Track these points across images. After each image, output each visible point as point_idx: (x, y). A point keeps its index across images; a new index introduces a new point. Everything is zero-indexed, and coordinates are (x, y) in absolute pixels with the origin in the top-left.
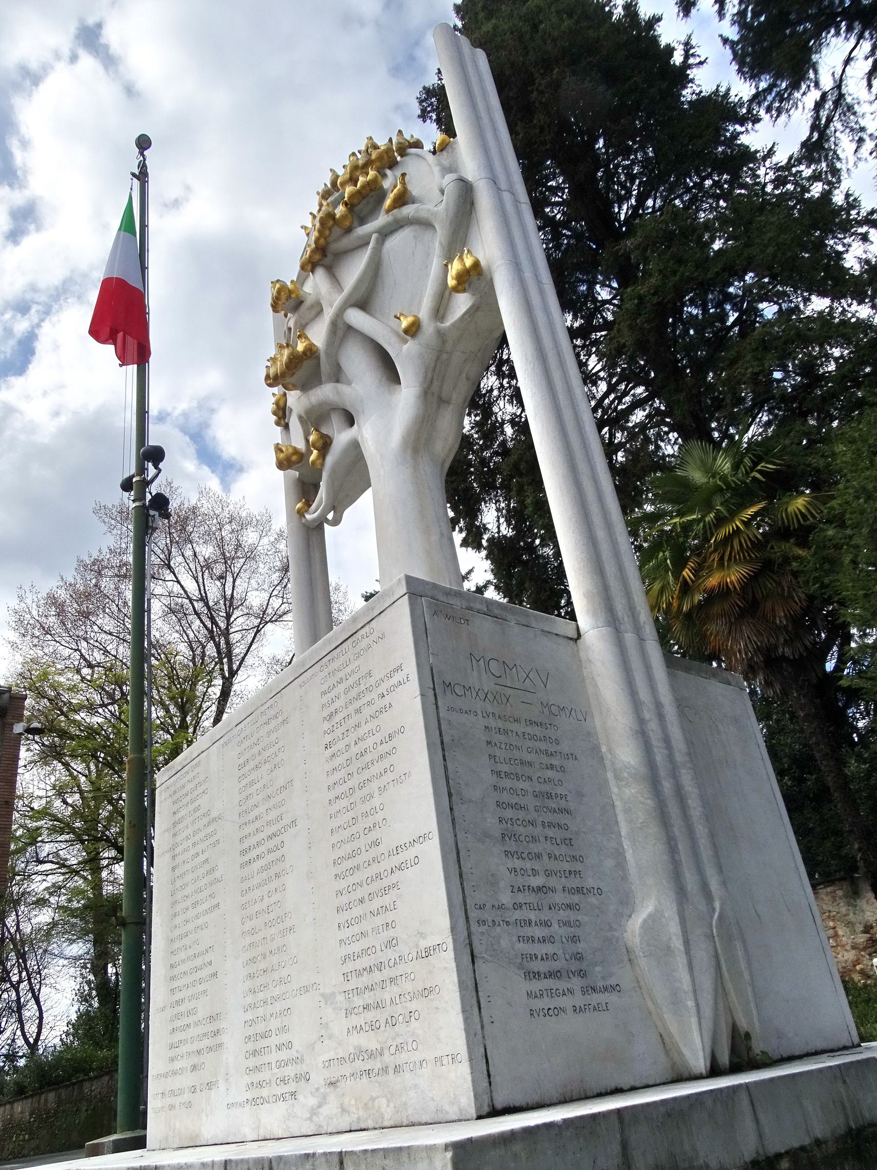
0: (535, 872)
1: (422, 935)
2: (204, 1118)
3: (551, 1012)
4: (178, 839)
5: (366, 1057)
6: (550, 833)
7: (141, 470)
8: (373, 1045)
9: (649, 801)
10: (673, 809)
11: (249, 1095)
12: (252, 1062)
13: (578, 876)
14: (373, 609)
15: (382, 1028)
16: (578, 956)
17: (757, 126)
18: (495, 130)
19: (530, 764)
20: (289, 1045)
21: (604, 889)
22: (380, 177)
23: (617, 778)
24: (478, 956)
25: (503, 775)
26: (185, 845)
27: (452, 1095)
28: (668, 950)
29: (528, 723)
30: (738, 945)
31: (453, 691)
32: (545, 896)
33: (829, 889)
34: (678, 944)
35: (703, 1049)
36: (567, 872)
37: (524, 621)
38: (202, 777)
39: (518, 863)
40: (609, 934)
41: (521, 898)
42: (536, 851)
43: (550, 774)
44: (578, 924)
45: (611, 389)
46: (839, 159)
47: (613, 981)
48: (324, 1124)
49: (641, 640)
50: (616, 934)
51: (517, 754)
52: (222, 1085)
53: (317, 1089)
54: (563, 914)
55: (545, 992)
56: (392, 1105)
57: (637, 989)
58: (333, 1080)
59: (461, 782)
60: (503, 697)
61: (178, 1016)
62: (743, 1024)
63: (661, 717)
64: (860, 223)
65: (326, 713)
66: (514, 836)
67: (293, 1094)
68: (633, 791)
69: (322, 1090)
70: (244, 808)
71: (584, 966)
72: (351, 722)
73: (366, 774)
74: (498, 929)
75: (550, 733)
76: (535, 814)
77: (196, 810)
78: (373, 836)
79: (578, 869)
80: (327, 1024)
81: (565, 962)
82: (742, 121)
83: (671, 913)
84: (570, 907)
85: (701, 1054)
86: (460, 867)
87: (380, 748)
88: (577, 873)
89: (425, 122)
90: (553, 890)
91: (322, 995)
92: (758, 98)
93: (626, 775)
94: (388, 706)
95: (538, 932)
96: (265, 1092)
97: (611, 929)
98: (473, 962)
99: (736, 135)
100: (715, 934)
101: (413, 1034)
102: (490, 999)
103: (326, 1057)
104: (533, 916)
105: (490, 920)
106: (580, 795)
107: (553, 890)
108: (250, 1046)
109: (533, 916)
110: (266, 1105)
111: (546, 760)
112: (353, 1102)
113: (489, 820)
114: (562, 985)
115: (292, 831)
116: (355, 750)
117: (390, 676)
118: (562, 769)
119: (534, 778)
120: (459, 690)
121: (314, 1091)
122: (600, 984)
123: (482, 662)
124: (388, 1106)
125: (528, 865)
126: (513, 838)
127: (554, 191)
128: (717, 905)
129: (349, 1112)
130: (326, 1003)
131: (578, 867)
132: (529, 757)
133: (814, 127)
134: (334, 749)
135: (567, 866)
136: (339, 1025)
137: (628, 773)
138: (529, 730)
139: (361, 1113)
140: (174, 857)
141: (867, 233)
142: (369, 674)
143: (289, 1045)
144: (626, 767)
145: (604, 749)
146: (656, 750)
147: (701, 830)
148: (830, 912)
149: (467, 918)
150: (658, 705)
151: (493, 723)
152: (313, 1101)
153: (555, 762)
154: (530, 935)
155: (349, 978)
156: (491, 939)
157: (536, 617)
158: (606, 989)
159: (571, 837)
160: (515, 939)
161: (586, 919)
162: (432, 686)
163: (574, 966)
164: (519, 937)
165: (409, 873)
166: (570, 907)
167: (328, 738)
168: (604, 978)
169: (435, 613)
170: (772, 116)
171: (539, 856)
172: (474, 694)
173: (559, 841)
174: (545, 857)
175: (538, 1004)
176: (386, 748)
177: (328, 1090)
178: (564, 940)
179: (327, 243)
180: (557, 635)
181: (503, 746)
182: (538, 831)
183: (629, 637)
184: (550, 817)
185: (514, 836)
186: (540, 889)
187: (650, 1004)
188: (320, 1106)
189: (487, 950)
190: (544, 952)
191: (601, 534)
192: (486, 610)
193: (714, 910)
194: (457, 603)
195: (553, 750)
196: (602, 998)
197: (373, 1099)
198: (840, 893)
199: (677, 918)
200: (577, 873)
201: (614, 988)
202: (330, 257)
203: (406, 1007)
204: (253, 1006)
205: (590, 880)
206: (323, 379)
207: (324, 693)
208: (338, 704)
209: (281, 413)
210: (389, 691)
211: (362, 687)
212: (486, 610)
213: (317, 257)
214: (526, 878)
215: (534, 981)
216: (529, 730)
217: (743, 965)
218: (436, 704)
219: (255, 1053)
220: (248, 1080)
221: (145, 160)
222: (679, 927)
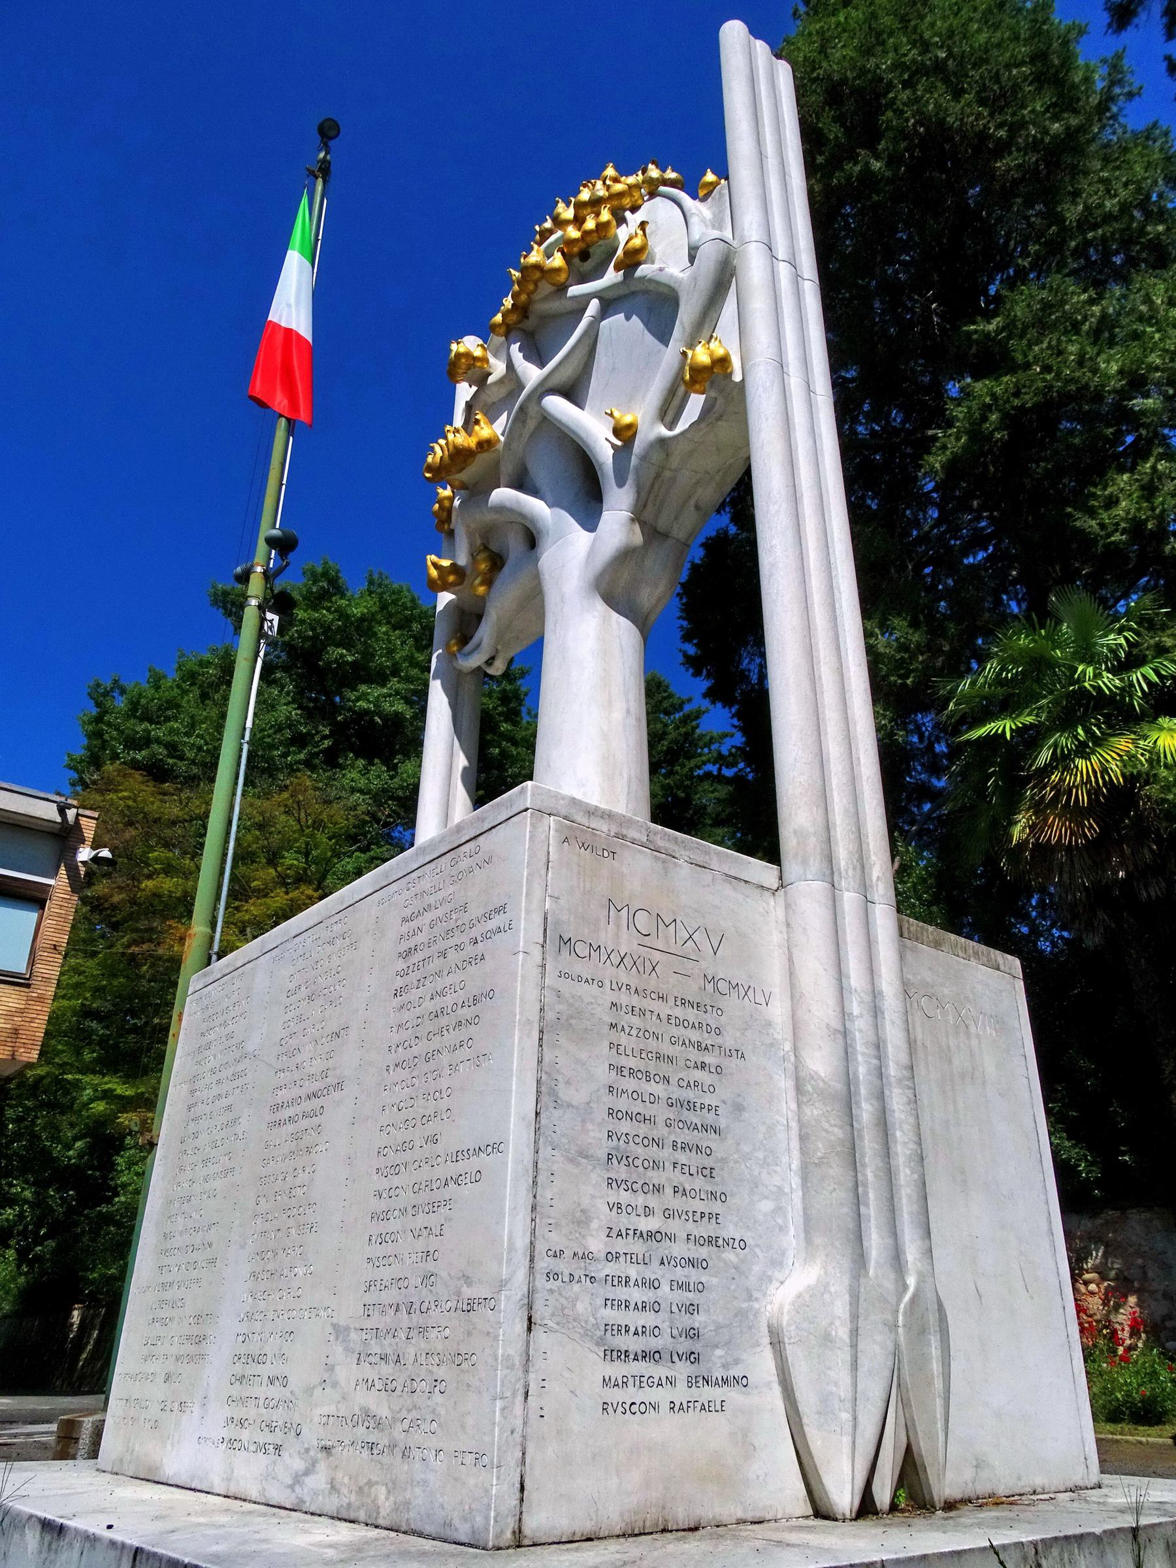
0: (648, 1211)
1: (468, 1280)
2: (169, 1447)
5: (372, 1425)
6: (682, 1157)
8: (384, 1412)
9: (836, 1130)
10: (869, 1144)
11: (225, 1433)
12: (236, 1390)
14: (483, 820)
15: (398, 1392)
16: (692, 1332)
20: (284, 1381)
21: (750, 1242)
22: (614, 223)
24: (539, 1322)
25: (626, 1073)
27: (467, 1507)
29: (679, 1003)
30: (934, 1341)
34: (842, 1332)
36: (698, 1215)
37: (700, 859)
39: (624, 1197)
40: (745, 1305)
41: (620, 1246)
43: (698, 1075)
47: (737, 1372)
48: (307, 1499)
49: (867, 901)
50: (756, 1306)
51: (652, 1044)
52: (196, 1409)
53: (307, 1450)
54: (680, 1274)
55: (631, 1380)
56: (392, 1499)
58: (329, 1443)
59: (560, 1078)
60: (647, 963)
61: (163, 1303)
63: (876, 1011)
66: (628, 1160)
67: (278, 1448)
68: (815, 1112)
69: (312, 1453)
71: (698, 1347)
72: (432, 967)
73: (436, 1042)
74: (576, 1287)
75: (710, 1019)
77: (230, 1036)
78: (431, 1128)
79: (715, 1210)
80: (333, 1366)
81: (671, 1340)
83: (840, 1286)
84: (691, 1262)
85: (849, 1487)
87: (460, 1011)
88: (714, 1217)
90: (671, 1238)
91: (334, 1326)
94: (479, 957)
95: (637, 1295)
96: (245, 1435)
97: (750, 1298)
98: (529, 1329)
100: (900, 1323)
101: (434, 1411)
102: (544, 1384)
103: (326, 1410)
104: (633, 1272)
105: (566, 1273)
106: (739, 1108)
107: (671, 1238)
108: (238, 1369)
109: (633, 1272)
110: (243, 1453)
111: (694, 1055)
112: (346, 1480)
113: (592, 1134)
115: (336, 1095)
116: (429, 1006)
118: (719, 1071)
119: (673, 1081)
120: (582, 949)
121: (302, 1451)
122: (718, 1373)
123: (624, 912)
124: (387, 1499)
125: (640, 1200)
126: (624, 1161)
128: (911, 1281)
129: (339, 1493)
130: (337, 1338)
131: (717, 1207)
132: (670, 1050)
134: (405, 998)
135: (699, 1206)
136: (347, 1372)
137: (812, 1086)
138: (678, 1012)
139: (353, 1498)
140: (193, 1092)
143: (284, 1381)
144: (812, 1077)
146: (860, 1058)
147: (905, 1175)
148: (1140, 1245)
149: (531, 1268)
150: (875, 995)
151: (624, 999)
152: (298, 1465)
153: (709, 1059)
154: (623, 1298)
155: (371, 1312)
156: (563, 1301)
157: (718, 854)
158: (725, 1381)
160: (600, 1302)
161: (715, 1281)
162: (541, 941)
163: (684, 1346)
165: (467, 1190)
166: (691, 1262)
167: (399, 982)
168: (725, 1366)
169: (566, 840)
171: (658, 1189)
172: (604, 957)
174: (669, 1191)
175: (617, 1395)
176: (465, 1013)
177: (320, 1455)
178: (675, 1309)
179: (530, 301)
182: (666, 1154)
183: (850, 899)
184: (686, 1136)
185: (628, 1160)
186: (651, 1235)
188: (307, 1473)
189: (553, 1315)
190: (641, 1323)
191: (834, 749)
192: (644, 839)
193: (905, 1287)
194: (603, 826)
195: (709, 1042)
197: (370, 1484)
199: (847, 1297)
200: (714, 1217)
203: (431, 1372)
205: (731, 1227)
206: (502, 481)
207: (405, 920)
208: (421, 938)
210: (486, 937)
211: (452, 924)
212: (644, 839)
215: (617, 1363)
216: (678, 1012)
217: (936, 1366)
218: (543, 966)
219: (241, 1379)
220: (228, 1412)
222: (848, 1308)
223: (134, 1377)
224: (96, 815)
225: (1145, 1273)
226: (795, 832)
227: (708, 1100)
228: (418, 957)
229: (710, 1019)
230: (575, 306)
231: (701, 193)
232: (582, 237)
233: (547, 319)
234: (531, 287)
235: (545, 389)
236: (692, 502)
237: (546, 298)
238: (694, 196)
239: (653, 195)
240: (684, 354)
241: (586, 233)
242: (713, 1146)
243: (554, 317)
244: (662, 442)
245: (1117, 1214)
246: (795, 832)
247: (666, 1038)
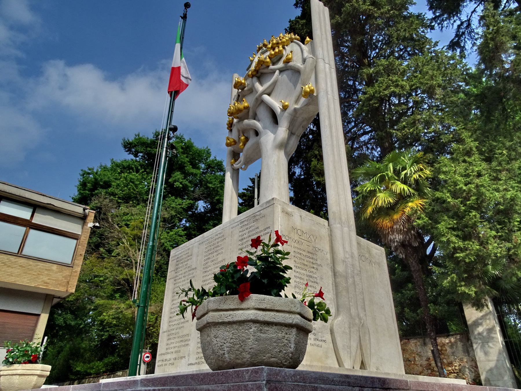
4: (178, 274)
17: (432, 31)
18: (327, 39)
19: (307, 265)
26: (180, 276)
38: (190, 254)
43: (312, 270)
45: (356, 125)
47: (324, 339)
51: (303, 261)
65: (240, 238)
70: (205, 266)
75: (314, 257)
77: (186, 265)
82: (426, 26)
92: (434, 19)
111: (312, 265)
117: (265, 230)
119: (307, 270)
122: (320, 339)
127: (346, 41)
133: (457, 35)
142: (258, 228)
151: (296, 250)
153: (315, 266)
167: (240, 247)
170: (439, 27)
179: (259, 69)
196: (320, 343)
198: (418, 343)
202: (259, 74)
204: (187, 340)
206: (250, 117)
207: (240, 232)
208: (245, 236)
209: (230, 126)
216: (307, 254)
221: (187, 12)
223: (161, 354)
224: (94, 212)
225: (415, 359)
226: (333, 212)
227: (315, 276)
228: (245, 241)
229: (314, 257)
230: (271, 71)
231: (305, 43)
232: (275, 53)
233: (262, 74)
234: (260, 66)
235: (263, 93)
236: (301, 126)
237: (264, 69)
238: (304, 44)
239: (292, 42)
240: (302, 88)
241: (276, 53)
242: (317, 287)
243: (265, 73)
244: (295, 110)
245: (407, 340)
246: (333, 212)
247: (306, 260)
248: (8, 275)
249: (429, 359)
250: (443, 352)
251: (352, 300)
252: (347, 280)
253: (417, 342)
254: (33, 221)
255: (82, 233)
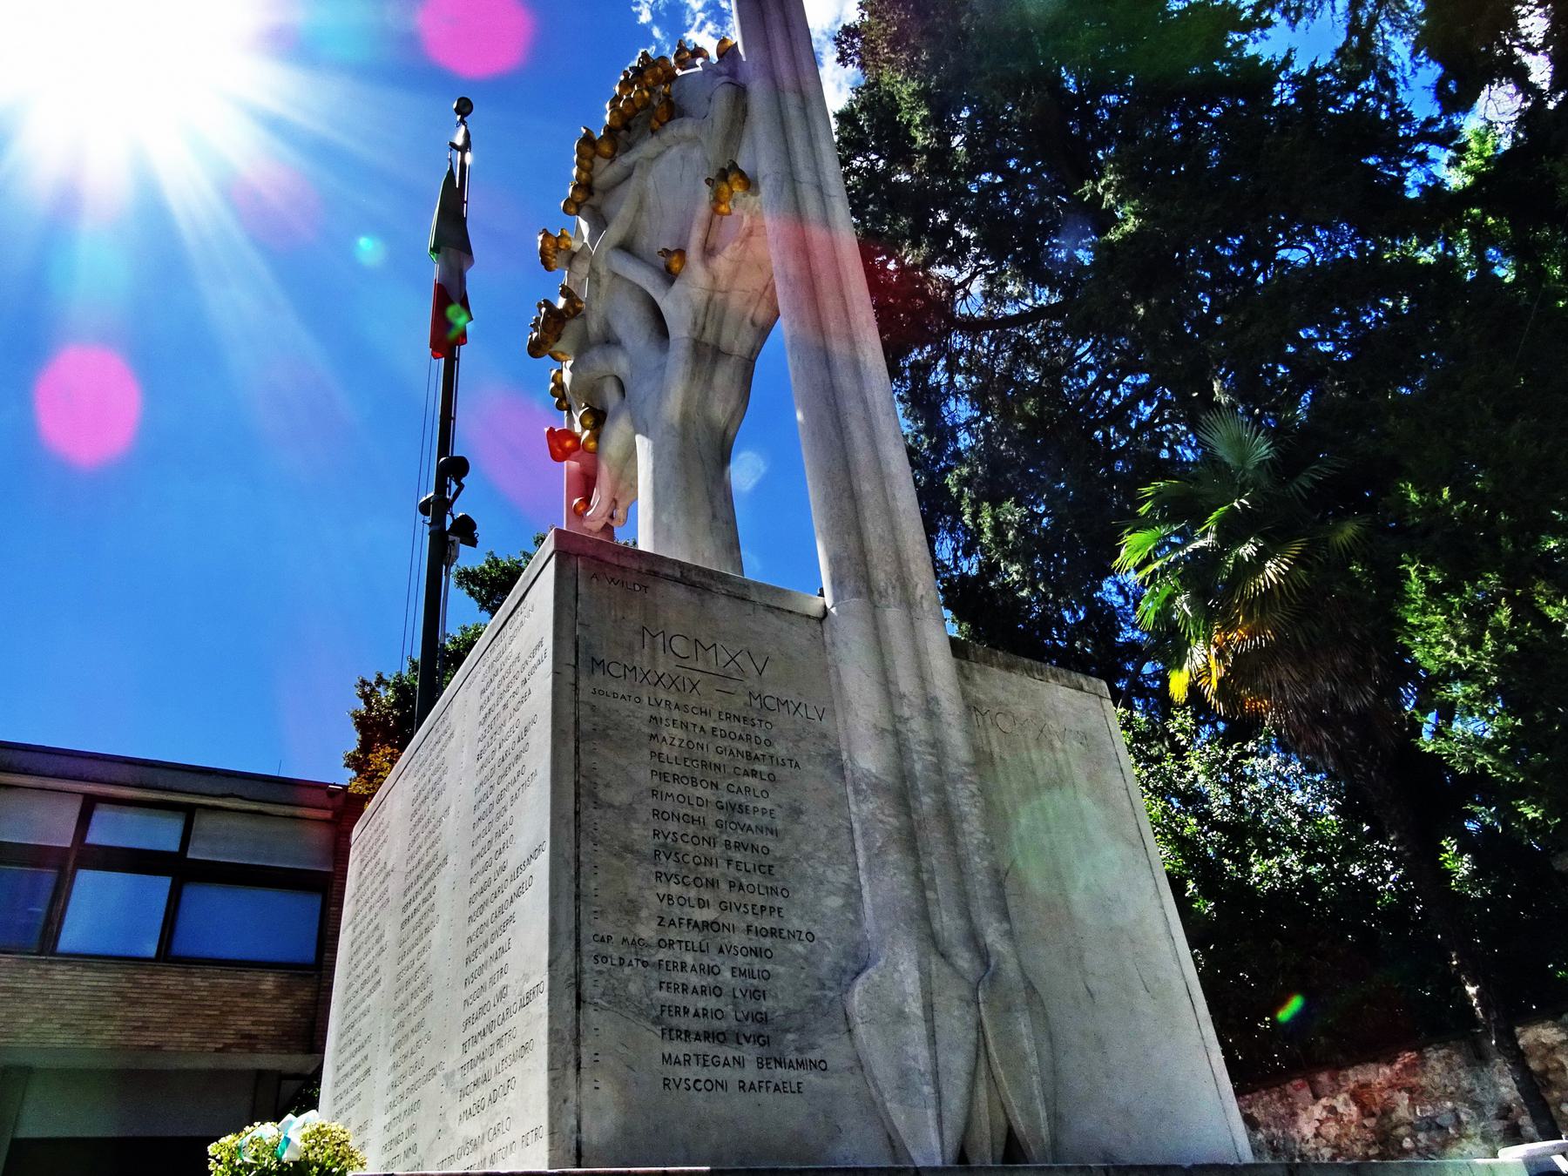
0: (702, 904)
3: (699, 1085)
6: (737, 856)
7: (441, 487)
13: (776, 914)
17: (1268, 32)
21: (818, 935)
23: (857, 792)
24: (588, 1000)
28: (901, 1016)
29: (723, 717)
31: (606, 670)
32: (716, 934)
33: (1442, 1053)
34: (914, 1008)
35: (943, 1152)
42: (709, 876)
44: (767, 976)
46: (1393, 68)
47: (814, 1056)
57: (858, 1071)
62: (1021, 1124)
64: (1417, 140)
74: (627, 970)
76: (716, 831)
81: (735, 1023)
82: (1246, 27)
84: (756, 952)
86: (578, 886)
89: (845, 66)
93: (864, 787)
99: (1239, 46)
102: (597, 1058)
105: (616, 955)
114: (728, 1052)
122: (792, 1056)
125: (693, 893)
131: (779, 902)
133: (1353, 29)
137: (867, 784)
138: (724, 725)
141: (1424, 153)
145: (845, 756)
154: (680, 981)
159: (771, 863)
160: (653, 984)
163: (750, 1028)
164: (661, 983)
166: (756, 952)
171: (712, 884)
172: (640, 677)
173: (750, 867)
174: (724, 886)
179: (591, 178)
180: (790, 612)
181: (676, 742)
186: (706, 925)
187: (873, 1090)
189: (604, 994)
201: (819, 1066)
213: (579, 197)
214: (687, 909)
216: (724, 725)
225: (1458, 1117)
248: (135, 1028)
249: (1509, 1109)
250: (1551, 1077)
251: (937, 881)
252: (908, 806)
253: (1450, 1056)
254: (190, 856)
255: (334, 867)
